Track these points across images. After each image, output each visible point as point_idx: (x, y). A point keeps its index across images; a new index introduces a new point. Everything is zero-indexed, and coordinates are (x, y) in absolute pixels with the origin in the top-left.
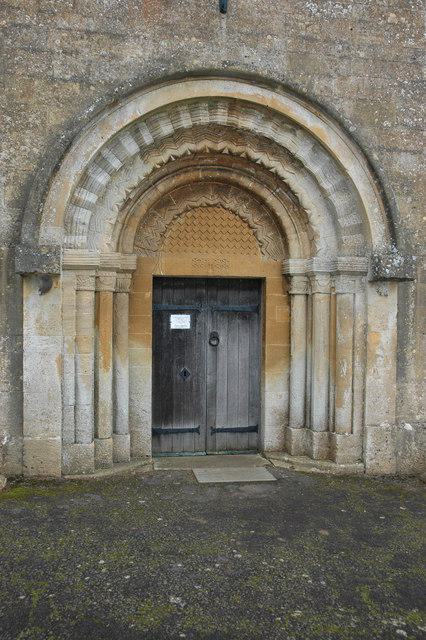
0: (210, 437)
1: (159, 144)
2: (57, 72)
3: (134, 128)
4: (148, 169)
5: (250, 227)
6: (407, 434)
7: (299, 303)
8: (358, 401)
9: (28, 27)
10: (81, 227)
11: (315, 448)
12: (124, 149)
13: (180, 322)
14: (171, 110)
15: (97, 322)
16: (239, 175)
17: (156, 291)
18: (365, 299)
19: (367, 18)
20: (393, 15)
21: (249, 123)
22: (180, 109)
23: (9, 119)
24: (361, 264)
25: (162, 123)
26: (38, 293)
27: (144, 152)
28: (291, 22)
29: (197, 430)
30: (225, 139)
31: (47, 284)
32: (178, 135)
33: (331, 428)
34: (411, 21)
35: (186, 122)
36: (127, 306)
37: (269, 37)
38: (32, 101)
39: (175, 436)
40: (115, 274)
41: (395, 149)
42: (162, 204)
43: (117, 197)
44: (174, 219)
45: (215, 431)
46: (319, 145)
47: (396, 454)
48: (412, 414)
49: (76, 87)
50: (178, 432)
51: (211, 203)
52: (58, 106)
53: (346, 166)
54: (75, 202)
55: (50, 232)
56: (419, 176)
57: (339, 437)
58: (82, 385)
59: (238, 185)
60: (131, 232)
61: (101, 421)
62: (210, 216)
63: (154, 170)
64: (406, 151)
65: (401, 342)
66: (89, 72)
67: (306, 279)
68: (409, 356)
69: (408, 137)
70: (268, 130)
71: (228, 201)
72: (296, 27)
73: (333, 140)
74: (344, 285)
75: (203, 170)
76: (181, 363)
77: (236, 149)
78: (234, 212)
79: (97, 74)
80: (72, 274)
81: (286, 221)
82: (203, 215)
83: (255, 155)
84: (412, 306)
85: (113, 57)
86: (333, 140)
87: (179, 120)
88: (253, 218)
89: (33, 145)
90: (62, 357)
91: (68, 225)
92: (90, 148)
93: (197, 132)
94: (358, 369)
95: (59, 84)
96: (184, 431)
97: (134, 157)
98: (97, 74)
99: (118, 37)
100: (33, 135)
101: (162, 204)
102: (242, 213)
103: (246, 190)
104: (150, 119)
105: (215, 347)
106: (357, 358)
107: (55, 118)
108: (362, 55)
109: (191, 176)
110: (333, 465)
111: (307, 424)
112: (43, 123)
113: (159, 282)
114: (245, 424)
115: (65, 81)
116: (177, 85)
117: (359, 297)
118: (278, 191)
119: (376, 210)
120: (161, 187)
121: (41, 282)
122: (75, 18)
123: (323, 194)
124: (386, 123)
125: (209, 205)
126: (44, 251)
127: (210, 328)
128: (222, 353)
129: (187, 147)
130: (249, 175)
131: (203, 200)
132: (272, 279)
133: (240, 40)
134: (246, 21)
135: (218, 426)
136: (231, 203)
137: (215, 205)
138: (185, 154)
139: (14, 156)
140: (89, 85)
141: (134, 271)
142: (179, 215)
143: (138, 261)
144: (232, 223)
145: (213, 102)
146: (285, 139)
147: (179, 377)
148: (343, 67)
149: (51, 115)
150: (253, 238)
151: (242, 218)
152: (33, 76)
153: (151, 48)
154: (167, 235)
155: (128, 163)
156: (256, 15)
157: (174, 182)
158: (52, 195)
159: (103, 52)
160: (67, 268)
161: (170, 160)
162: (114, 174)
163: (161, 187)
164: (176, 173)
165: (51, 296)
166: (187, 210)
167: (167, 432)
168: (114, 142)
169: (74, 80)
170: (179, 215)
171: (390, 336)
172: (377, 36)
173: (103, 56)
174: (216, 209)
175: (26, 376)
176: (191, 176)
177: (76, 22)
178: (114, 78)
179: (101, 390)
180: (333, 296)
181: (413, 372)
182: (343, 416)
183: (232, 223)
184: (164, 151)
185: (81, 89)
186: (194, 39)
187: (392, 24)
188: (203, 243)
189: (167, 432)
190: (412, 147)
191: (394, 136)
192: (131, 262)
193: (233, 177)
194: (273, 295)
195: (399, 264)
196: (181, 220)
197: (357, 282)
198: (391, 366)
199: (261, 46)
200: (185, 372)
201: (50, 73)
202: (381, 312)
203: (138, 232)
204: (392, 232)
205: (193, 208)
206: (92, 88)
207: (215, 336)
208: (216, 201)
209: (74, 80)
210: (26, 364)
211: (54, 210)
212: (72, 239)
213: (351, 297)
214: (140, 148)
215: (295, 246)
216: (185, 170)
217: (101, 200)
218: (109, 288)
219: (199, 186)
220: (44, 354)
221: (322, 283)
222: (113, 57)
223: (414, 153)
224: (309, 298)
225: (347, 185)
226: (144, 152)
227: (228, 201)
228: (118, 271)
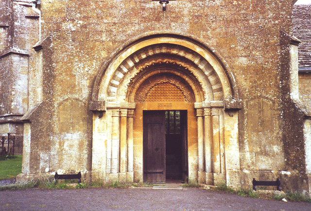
1: (142, 61)
3: (131, 57)
4: (138, 71)
7: (200, 119)
8: (222, 159)
10: (113, 94)
11: (207, 180)
14: (145, 50)
15: (120, 128)
16: (175, 71)
18: (223, 119)
23: (88, 56)
24: (220, 103)
27: (136, 65)
28: (191, 11)
31: (101, 114)
33: (213, 171)
35: (151, 53)
36: (132, 122)
39: (153, 174)
40: (126, 110)
42: (146, 83)
43: (127, 81)
46: (202, 59)
50: (154, 173)
53: (212, 65)
54: (111, 84)
55: (102, 96)
64: (242, 56)
65: (241, 135)
67: (202, 110)
70: (182, 54)
73: (207, 56)
74: (214, 111)
75: (161, 69)
77: (171, 61)
80: (111, 110)
81: (194, 87)
83: (179, 63)
86: (207, 56)
88: (182, 87)
89: (96, 65)
91: (109, 93)
93: (155, 56)
94: (222, 147)
96: (157, 173)
97: (133, 67)
101: (146, 83)
103: (178, 76)
104: (137, 53)
106: (221, 141)
107: (104, 54)
111: (204, 170)
113: (145, 113)
117: (221, 116)
119: (226, 82)
122: (110, 19)
123: (206, 78)
125: (164, 83)
132: (190, 110)
134: (173, 12)
135: (133, 111)
136: (172, 82)
138: (135, 76)
139: (90, 70)
141: (135, 109)
142: (153, 87)
143: (137, 105)
145: (161, 46)
146: (189, 57)
148: (213, 25)
151: (177, 87)
154: (148, 95)
155: (130, 70)
156: (177, 10)
158: (102, 83)
160: (108, 109)
162: (125, 74)
164: (146, 73)
165: (103, 119)
168: (124, 63)
177: (110, 20)
179: (121, 154)
180: (211, 116)
181: (248, 147)
182: (217, 165)
188: (162, 97)
192: (133, 106)
194: (190, 117)
196: (153, 89)
197: (220, 111)
201: (102, 39)
202: (231, 125)
203: (137, 94)
204: (232, 91)
205: (158, 84)
212: (110, 98)
213: (218, 117)
215: (197, 97)
218: (124, 115)
219: (161, 76)
221: (207, 111)
223: (245, 57)
224: (203, 117)
225: (213, 73)
228: (128, 109)
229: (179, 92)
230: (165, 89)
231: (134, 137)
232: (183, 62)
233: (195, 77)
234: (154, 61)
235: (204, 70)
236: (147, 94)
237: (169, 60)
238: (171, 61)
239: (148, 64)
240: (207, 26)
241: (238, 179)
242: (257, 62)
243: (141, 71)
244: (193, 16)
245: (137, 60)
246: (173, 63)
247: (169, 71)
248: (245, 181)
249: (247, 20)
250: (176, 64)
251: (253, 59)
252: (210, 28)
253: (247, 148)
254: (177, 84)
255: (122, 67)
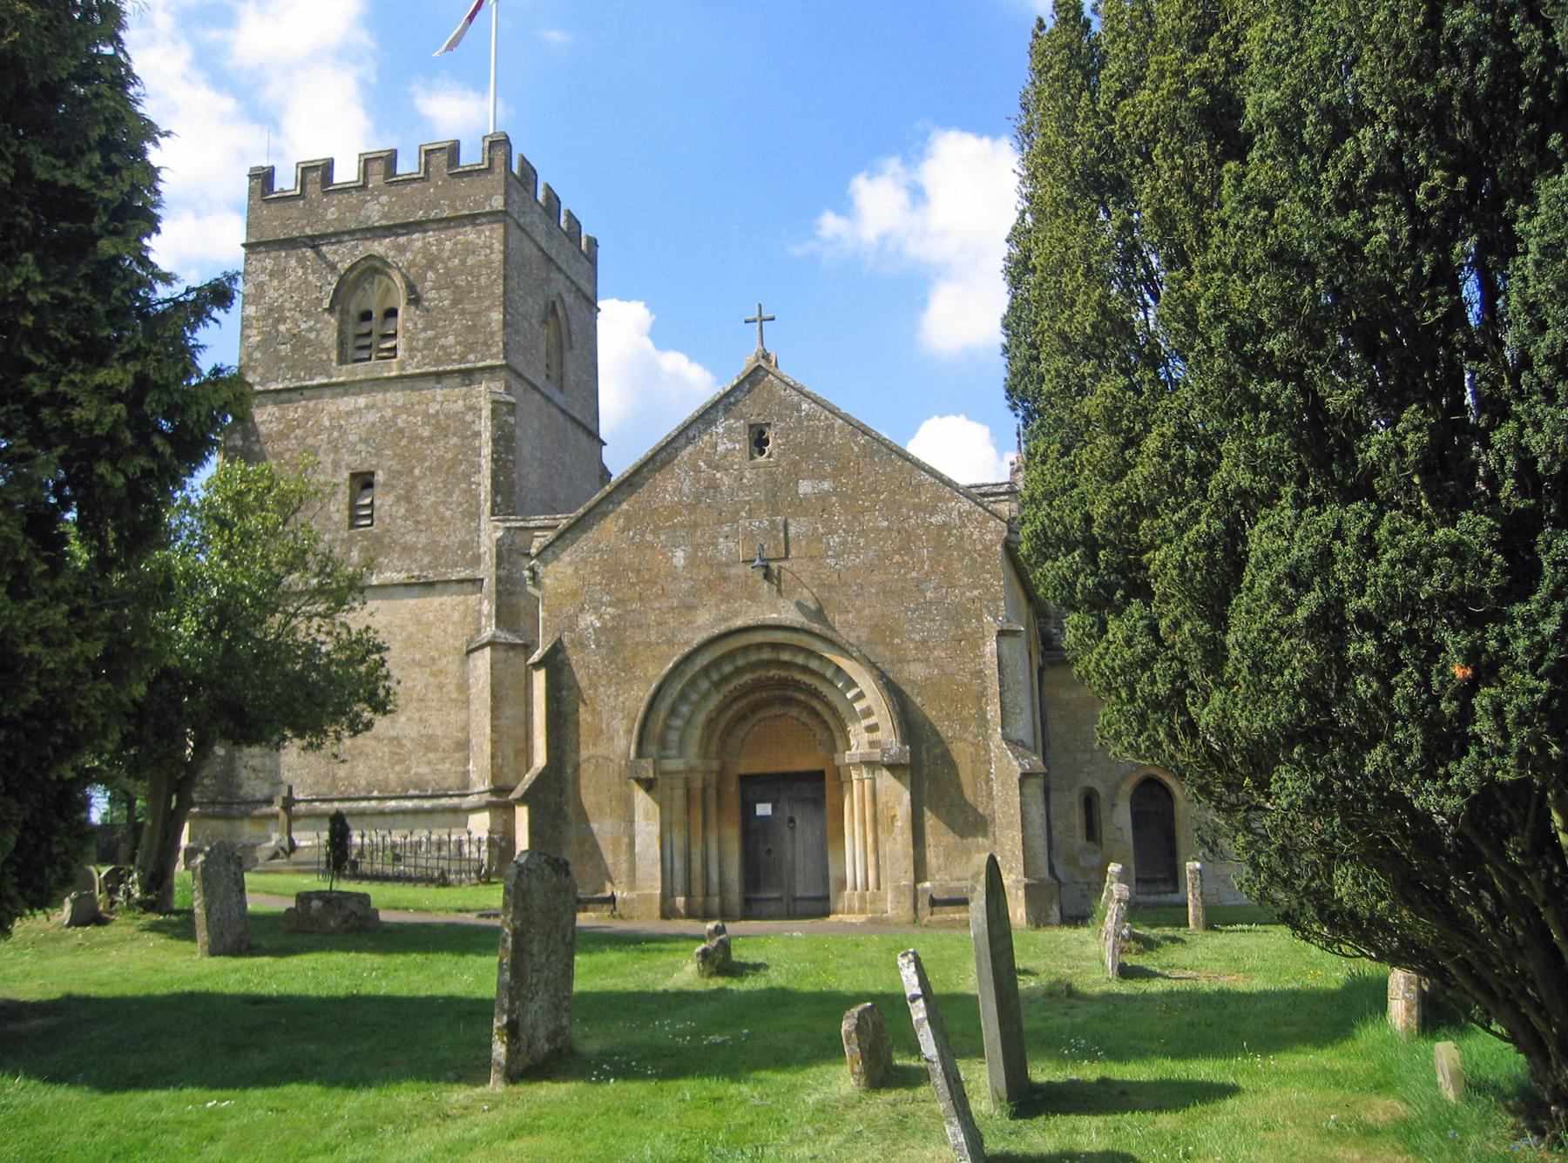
0: (791, 906)
1: (725, 679)
2: (653, 639)
9: (633, 611)
13: (764, 809)
17: (513, 784)
19: (876, 562)
21: (785, 656)
29: (780, 899)
32: (738, 671)
38: (638, 660)
45: (795, 899)
58: (676, 858)
60: (715, 741)
63: (725, 697)
72: (819, 578)
78: (798, 719)
83: (799, 676)
84: (927, 785)
88: (812, 723)
93: (738, 671)
99: (691, 608)
103: (800, 702)
105: (793, 829)
113: (746, 780)
114: (820, 894)
120: (735, 707)
124: (897, 641)
127: (788, 813)
128: (798, 833)
129: (747, 677)
135: (798, 895)
148: (858, 603)
153: (714, 611)
155: (705, 696)
157: (744, 702)
166: (759, 721)
167: (757, 900)
175: (637, 849)
177: (666, 604)
187: (898, 563)
189: (757, 900)
193: (790, 693)
198: (908, 835)
203: (723, 742)
207: (792, 820)
209: (664, 642)
210: (637, 841)
217: (689, 722)
226: (717, 685)
231: (719, 829)
254: (804, 717)
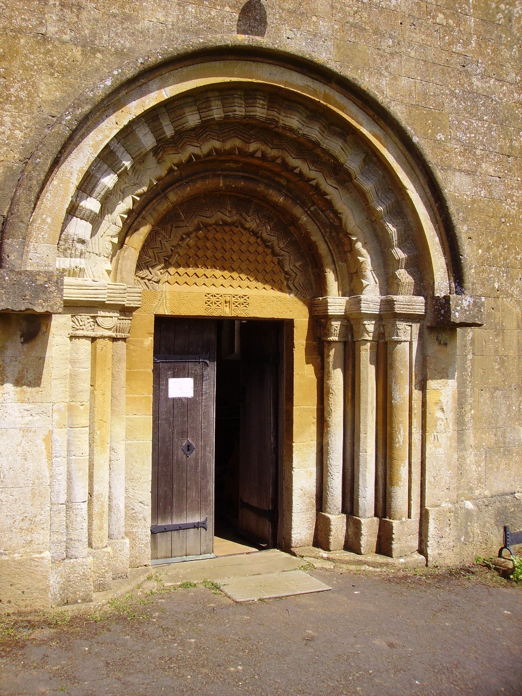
2: (51, 30)
4: (162, 172)
5: (274, 254)
6: (468, 513)
12: (138, 141)
16: (268, 186)
20: (441, 16)
22: (210, 94)
25: (187, 110)
26: (19, 340)
30: (257, 140)
34: (458, 25)
37: (314, 19)
39: (175, 533)
40: (409, 340)
41: (449, 167)
44: (182, 239)
47: (459, 539)
48: (471, 489)
49: (77, 53)
51: (229, 220)
52: (52, 74)
56: (474, 201)
57: (395, 523)
59: (264, 199)
61: (96, 522)
62: (227, 237)
64: (460, 171)
66: (94, 35)
68: (468, 417)
69: (462, 154)
71: (249, 219)
76: (184, 434)
77: (272, 152)
79: (105, 37)
82: (219, 236)
83: (294, 162)
84: (470, 357)
85: (127, 18)
87: (209, 108)
90: (51, 432)
92: (100, 137)
95: (55, 46)
98: (105, 37)
100: (15, 112)
102: (265, 235)
103: (275, 206)
108: (412, 54)
109: (209, 184)
110: (389, 560)
112: (29, 95)
115: (64, 43)
116: (213, 63)
118: (312, 209)
120: (173, 197)
121: (24, 324)
125: (225, 223)
126: (41, 280)
130: (279, 187)
131: (219, 216)
133: (281, 17)
137: (233, 224)
140: (95, 51)
142: (188, 235)
144: (252, 249)
147: (180, 453)
149: (43, 88)
150: (277, 269)
151: (264, 241)
152: (20, 31)
153: (175, 12)
159: (114, 10)
161: (190, 160)
163: (173, 197)
169: (75, 42)
170: (188, 235)
171: (450, 393)
172: (427, 35)
173: (114, 16)
174: (234, 228)
176: (209, 184)
178: (128, 45)
183: (252, 249)
184: (183, 148)
185: (84, 54)
186: (227, 9)
190: (465, 166)
191: (448, 152)
193: (261, 188)
195: (468, 306)
199: (304, 27)
200: (189, 447)
206: (99, 55)
208: (235, 218)
209: (75, 42)
211: (49, 220)
214: (158, 141)
216: (202, 175)
220: (26, 430)
222: (127, 18)
223: (468, 173)
227: (249, 219)
229: (269, 258)
230: (227, 247)
232: (305, 160)
233: (336, 213)
234: (217, 144)
235: (372, 196)
236: (170, 257)
237: (264, 148)
238: (272, 152)
239: (197, 151)
240: (378, 61)
241: (454, 533)
242: (490, 192)
243: (170, 171)
244: (343, 23)
245: (169, 131)
246: (273, 159)
247: (251, 185)
248: (467, 534)
249: (468, 75)
250: (285, 164)
251: (484, 184)
252: (386, 68)
253: (470, 438)
254: (266, 232)
255: (120, 151)
